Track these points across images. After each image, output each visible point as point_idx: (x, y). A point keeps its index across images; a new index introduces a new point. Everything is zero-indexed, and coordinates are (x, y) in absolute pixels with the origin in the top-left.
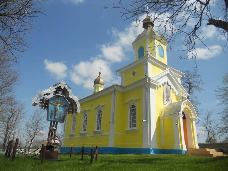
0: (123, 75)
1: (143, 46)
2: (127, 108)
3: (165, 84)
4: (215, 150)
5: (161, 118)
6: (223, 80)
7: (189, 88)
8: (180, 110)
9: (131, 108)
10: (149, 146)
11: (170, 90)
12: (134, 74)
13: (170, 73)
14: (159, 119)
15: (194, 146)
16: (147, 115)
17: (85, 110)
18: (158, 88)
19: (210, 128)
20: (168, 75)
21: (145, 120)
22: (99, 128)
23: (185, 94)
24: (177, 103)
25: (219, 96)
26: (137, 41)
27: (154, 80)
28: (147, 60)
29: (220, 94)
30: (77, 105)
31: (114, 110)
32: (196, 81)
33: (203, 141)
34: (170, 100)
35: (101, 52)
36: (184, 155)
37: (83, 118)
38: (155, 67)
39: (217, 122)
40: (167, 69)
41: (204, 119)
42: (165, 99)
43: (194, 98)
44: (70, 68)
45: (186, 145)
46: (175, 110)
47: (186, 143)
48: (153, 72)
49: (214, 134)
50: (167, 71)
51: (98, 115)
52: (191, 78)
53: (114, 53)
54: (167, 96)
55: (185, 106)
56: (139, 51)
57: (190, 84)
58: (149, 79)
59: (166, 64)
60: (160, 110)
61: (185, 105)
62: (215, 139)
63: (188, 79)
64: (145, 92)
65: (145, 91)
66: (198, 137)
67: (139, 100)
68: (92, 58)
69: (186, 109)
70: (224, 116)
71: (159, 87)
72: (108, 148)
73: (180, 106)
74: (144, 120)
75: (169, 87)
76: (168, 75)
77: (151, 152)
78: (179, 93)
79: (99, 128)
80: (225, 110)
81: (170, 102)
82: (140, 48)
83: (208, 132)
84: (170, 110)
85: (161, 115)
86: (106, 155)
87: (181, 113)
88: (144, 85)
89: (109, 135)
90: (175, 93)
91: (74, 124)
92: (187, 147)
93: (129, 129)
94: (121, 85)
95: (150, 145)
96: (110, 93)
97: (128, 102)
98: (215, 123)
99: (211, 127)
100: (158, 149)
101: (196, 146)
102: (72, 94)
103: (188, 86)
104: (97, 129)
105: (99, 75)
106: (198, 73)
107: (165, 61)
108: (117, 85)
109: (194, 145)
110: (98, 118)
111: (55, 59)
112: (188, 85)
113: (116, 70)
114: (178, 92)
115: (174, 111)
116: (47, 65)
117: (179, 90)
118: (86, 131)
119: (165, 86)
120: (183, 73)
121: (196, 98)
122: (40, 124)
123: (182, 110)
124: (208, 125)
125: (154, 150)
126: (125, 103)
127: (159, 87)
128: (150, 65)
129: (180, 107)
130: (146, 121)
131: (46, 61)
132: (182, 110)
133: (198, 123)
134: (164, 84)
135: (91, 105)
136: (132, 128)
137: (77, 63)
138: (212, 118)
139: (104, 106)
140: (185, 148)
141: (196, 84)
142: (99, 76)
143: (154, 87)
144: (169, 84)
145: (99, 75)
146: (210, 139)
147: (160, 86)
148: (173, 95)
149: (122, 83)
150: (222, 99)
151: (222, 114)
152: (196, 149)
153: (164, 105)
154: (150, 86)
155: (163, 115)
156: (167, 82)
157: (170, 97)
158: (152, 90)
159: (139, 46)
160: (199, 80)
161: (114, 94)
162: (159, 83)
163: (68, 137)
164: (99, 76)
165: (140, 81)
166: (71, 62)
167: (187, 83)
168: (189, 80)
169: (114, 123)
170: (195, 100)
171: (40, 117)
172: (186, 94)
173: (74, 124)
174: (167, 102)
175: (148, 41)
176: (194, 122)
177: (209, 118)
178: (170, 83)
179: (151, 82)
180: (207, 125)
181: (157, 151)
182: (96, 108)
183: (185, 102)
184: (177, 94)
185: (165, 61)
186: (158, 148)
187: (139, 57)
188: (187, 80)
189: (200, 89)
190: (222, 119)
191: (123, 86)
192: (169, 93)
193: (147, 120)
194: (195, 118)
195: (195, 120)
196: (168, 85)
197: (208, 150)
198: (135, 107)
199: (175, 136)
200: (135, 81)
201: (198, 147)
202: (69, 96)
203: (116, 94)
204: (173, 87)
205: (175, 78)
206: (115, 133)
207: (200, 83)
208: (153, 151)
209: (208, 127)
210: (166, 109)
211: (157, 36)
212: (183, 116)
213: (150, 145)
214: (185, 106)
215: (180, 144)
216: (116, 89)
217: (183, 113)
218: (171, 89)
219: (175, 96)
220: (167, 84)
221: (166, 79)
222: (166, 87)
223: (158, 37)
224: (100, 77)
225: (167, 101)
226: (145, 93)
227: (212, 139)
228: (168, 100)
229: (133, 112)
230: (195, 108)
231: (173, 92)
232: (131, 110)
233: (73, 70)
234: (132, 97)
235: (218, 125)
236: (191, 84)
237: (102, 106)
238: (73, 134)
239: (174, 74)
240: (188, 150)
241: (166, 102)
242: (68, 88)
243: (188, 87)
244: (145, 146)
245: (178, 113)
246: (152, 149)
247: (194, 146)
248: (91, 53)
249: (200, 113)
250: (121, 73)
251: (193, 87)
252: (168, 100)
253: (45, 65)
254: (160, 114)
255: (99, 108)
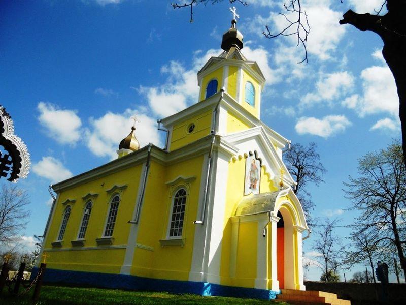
0: (171, 130)
1: (215, 79)
2: (170, 196)
3: (251, 155)
4: (336, 295)
5: (235, 222)
6: (359, 165)
7: (298, 176)
8: (273, 206)
9: (177, 195)
10: (202, 278)
11: (259, 168)
12: (191, 129)
13: (262, 135)
14: (231, 222)
15: (296, 284)
16: (206, 213)
17: (89, 194)
18: (234, 160)
19: (329, 253)
20: (258, 138)
21: (201, 222)
22: (109, 231)
23: (290, 181)
24: (270, 194)
25: (350, 193)
26: (206, 69)
27: (229, 142)
28: (219, 101)
29: (351, 191)
30: (22, 158)
31: (142, 197)
32: (312, 164)
33: (316, 277)
34: (257, 187)
35: (145, 102)
36: (272, 301)
37: (84, 210)
38: (234, 119)
39: (344, 242)
40: (257, 127)
41: (321, 236)
42: (248, 184)
43: (305, 195)
44: (86, 125)
45: (278, 281)
46: (263, 206)
47: (281, 278)
48: (228, 127)
49: (336, 265)
50: (258, 130)
51: (112, 206)
52: (303, 158)
53: (168, 103)
54: (252, 180)
55: (286, 201)
56: (207, 89)
57: (300, 168)
58: (218, 138)
59: (258, 117)
60: (236, 205)
61: (285, 198)
62: (337, 275)
63: (298, 160)
64: (208, 165)
65: (208, 161)
66: (305, 268)
67: (192, 180)
68: (129, 111)
69: (285, 207)
70: (356, 231)
71: (237, 158)
72: (119, 275)
73: (275, 199)
74: (197, 222)
75: (258, 161)
76: (258, 138)
77: (205, 292)
78: (276, 176)
79: (109, 231)
80: (359, 220)
81: (256, 192)
82: (209, 84)
83: (326, 261)
84: (254, 205)
85: (235, 214)
86: (94, 290)
87: (275, 213)
88: (206, 150)
89: (126, 248)
90: (268, 175)
91: (65, 222)
92: (282, 286)
93: (168, 239)
94: (164, 149)
95: (205, 276)
96: (140, 162)
97: (173, 184)
98: (339, 244)
99: (331, 252)
100: (220, 286)
101: (299, 286)
102: (13, 130)
103: (297, 173)
104: (105, 236)
105: (132, 132)
106: (317, 151)
107: (256, 112)
108: (153, 147)
109: (295, 283)
110: (111, 212)
111: (62, 104)
112: (297, 170)
113: (158, 120)
114: (276, 175)
115: (263, 208)
116: (43, 113)
117: (277, 169)
118: (84, 237)
119: (249, 158)
120: (288, 141)
121: (309, 194)
122: (9, 218)
123: (277, 207)
124: (327, 247)
125: (211, 287)
126: (167, 184)
127: (237, 158)
128: (223, 112)
129: (273, 201)
130: (202, 224)
131: (41, 106)
132: (277, 207)
133: (308, 237)
134: (248, 154)
135: (102, 185)
136: (173, 238)
137: (99, 115)
138: (334, 234)
139: (124, 188)
140: (275, 289)
141: (312, 171)
142: (131, 134)
143: (228, 156)
144: (259, 157)
145: (132, 132)
146: (328, 275)
147: (240, 158)
148: (264, 178)
149: (167, 146)
150: (354, 200)
151: (352, 227)
152: (299, 291)
153: (244, 195)
154: (219, 154)
155: (239, 214)
156: (255, 152)
157: (258, 181)
158: (221, 162)
159: (209, 79)
160: (317, 164)
161: (147, 165)
162: (238, 150)
163: (51, 249)
164: (131, 134)
165: (199, 142)
166: (89, 111)
167: (296, 166)
168: (299, 162)
169: (139, 223)
170: (307, 198)
171: (9, 207)
172: (289, 180)
173: (65, 222)
174: (250, 190)
175: (227, 70)
176: (300, 236)
177: (328, 234)
178: (260, 155)
179: (221, 145)
180: (324, 248)
181: (218, 290)
182: (110, 191)
183: (285, 193)
184: (272, 178)
185: (256, 112)
186: (224, 284)
187: (207, 97)
188: (296, 161)
189: (317, 180)
190: (351, 236)
191: (169, 150)
192: (256, 173)
193: (203, 222)
194: (302, 226)
195: (302, 231)
196: (257, 159)
197: (322, 294)
198: (185, 193)
199: (258, 263)
200: (191, 141)
201: (303, 288)
202: (4, 135)
203: (152, 164)
204: (265, 162)
205: (273, 148)
206: (137, 244)
207: (318, 170)
208: (209, 288)
209: (326, 251)
210: (247, 203)
211: (245, 64)
212: (278, 221)
213: (205, 276)
214: (286, 201)
215: (266, 278)
216: (151, 154)
217: (279, 214)
218: (261, 166)
219: (269, 181)
220: (254, 155)
221: (253, 146)
222: (252, 162)
223: (248, 67)
224: (133, 135)
225: (250, 188)
226: (208, 167)
227: (332, 275)
228: (253, 186)
229: (179, 204)
230: (307, 213)
231: (265, 174)
232: (176, 201)
233: (92, 129)
234: (182, 173)
235: (344, 247)
236: (302, 168)
237: (121, 187)
238: (59, 241)
239: (272, 140)
240: (281, 293)
241: (248, 191)
242: (3, 115)
243: (296, 174)
244: (193, 278)
245: (270, 212)
246: (208, 286)
247: (296, 284)
248: (128, 101)
249: (314, 223)
250: (168, 126)
251: (305, 174)
252: (253, 186)
253: (39, 113)
254: (234, 213)
255: (116, 191)
